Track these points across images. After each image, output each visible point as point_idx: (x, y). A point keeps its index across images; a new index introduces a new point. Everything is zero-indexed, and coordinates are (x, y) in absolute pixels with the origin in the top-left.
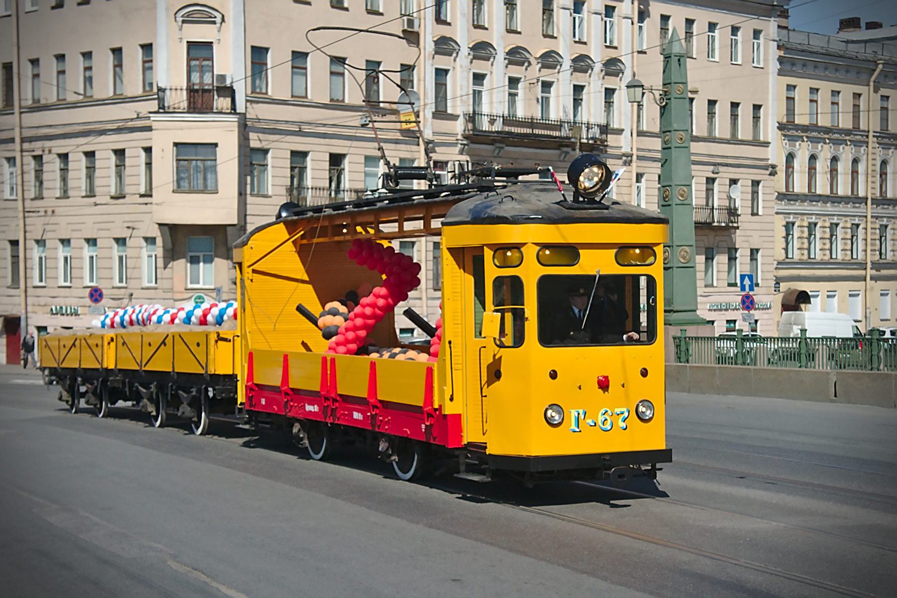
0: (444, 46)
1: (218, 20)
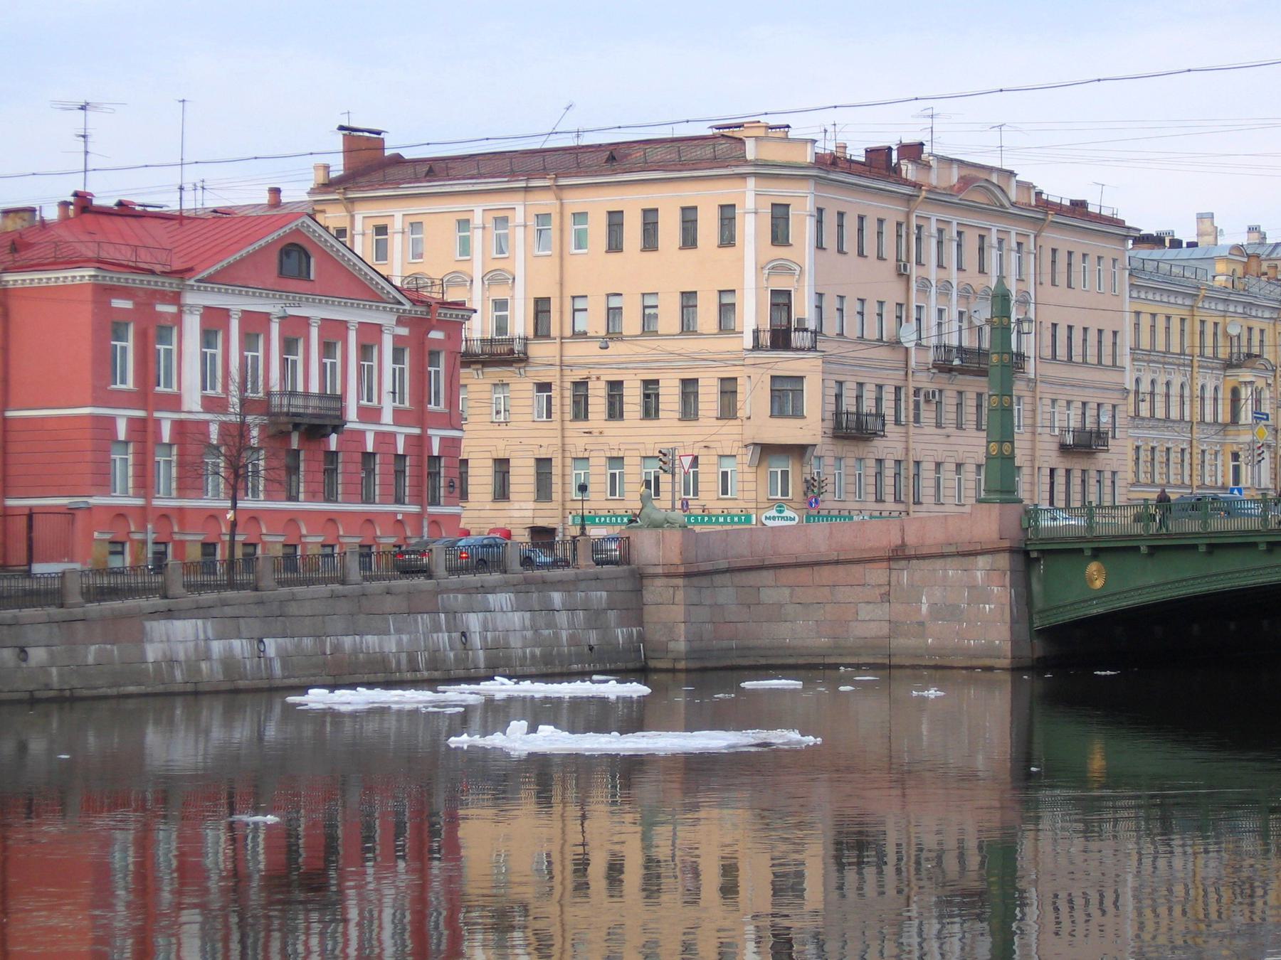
0: (945, 287)
1: (797, 272)
